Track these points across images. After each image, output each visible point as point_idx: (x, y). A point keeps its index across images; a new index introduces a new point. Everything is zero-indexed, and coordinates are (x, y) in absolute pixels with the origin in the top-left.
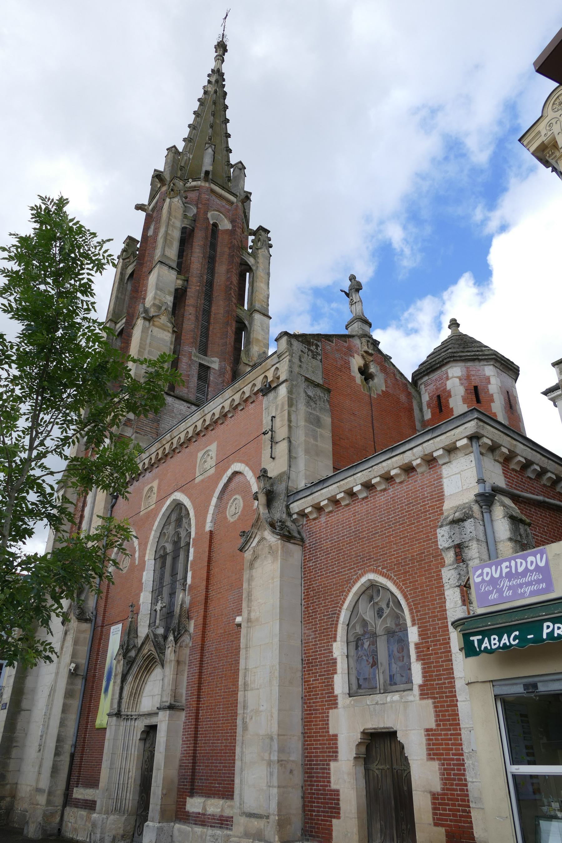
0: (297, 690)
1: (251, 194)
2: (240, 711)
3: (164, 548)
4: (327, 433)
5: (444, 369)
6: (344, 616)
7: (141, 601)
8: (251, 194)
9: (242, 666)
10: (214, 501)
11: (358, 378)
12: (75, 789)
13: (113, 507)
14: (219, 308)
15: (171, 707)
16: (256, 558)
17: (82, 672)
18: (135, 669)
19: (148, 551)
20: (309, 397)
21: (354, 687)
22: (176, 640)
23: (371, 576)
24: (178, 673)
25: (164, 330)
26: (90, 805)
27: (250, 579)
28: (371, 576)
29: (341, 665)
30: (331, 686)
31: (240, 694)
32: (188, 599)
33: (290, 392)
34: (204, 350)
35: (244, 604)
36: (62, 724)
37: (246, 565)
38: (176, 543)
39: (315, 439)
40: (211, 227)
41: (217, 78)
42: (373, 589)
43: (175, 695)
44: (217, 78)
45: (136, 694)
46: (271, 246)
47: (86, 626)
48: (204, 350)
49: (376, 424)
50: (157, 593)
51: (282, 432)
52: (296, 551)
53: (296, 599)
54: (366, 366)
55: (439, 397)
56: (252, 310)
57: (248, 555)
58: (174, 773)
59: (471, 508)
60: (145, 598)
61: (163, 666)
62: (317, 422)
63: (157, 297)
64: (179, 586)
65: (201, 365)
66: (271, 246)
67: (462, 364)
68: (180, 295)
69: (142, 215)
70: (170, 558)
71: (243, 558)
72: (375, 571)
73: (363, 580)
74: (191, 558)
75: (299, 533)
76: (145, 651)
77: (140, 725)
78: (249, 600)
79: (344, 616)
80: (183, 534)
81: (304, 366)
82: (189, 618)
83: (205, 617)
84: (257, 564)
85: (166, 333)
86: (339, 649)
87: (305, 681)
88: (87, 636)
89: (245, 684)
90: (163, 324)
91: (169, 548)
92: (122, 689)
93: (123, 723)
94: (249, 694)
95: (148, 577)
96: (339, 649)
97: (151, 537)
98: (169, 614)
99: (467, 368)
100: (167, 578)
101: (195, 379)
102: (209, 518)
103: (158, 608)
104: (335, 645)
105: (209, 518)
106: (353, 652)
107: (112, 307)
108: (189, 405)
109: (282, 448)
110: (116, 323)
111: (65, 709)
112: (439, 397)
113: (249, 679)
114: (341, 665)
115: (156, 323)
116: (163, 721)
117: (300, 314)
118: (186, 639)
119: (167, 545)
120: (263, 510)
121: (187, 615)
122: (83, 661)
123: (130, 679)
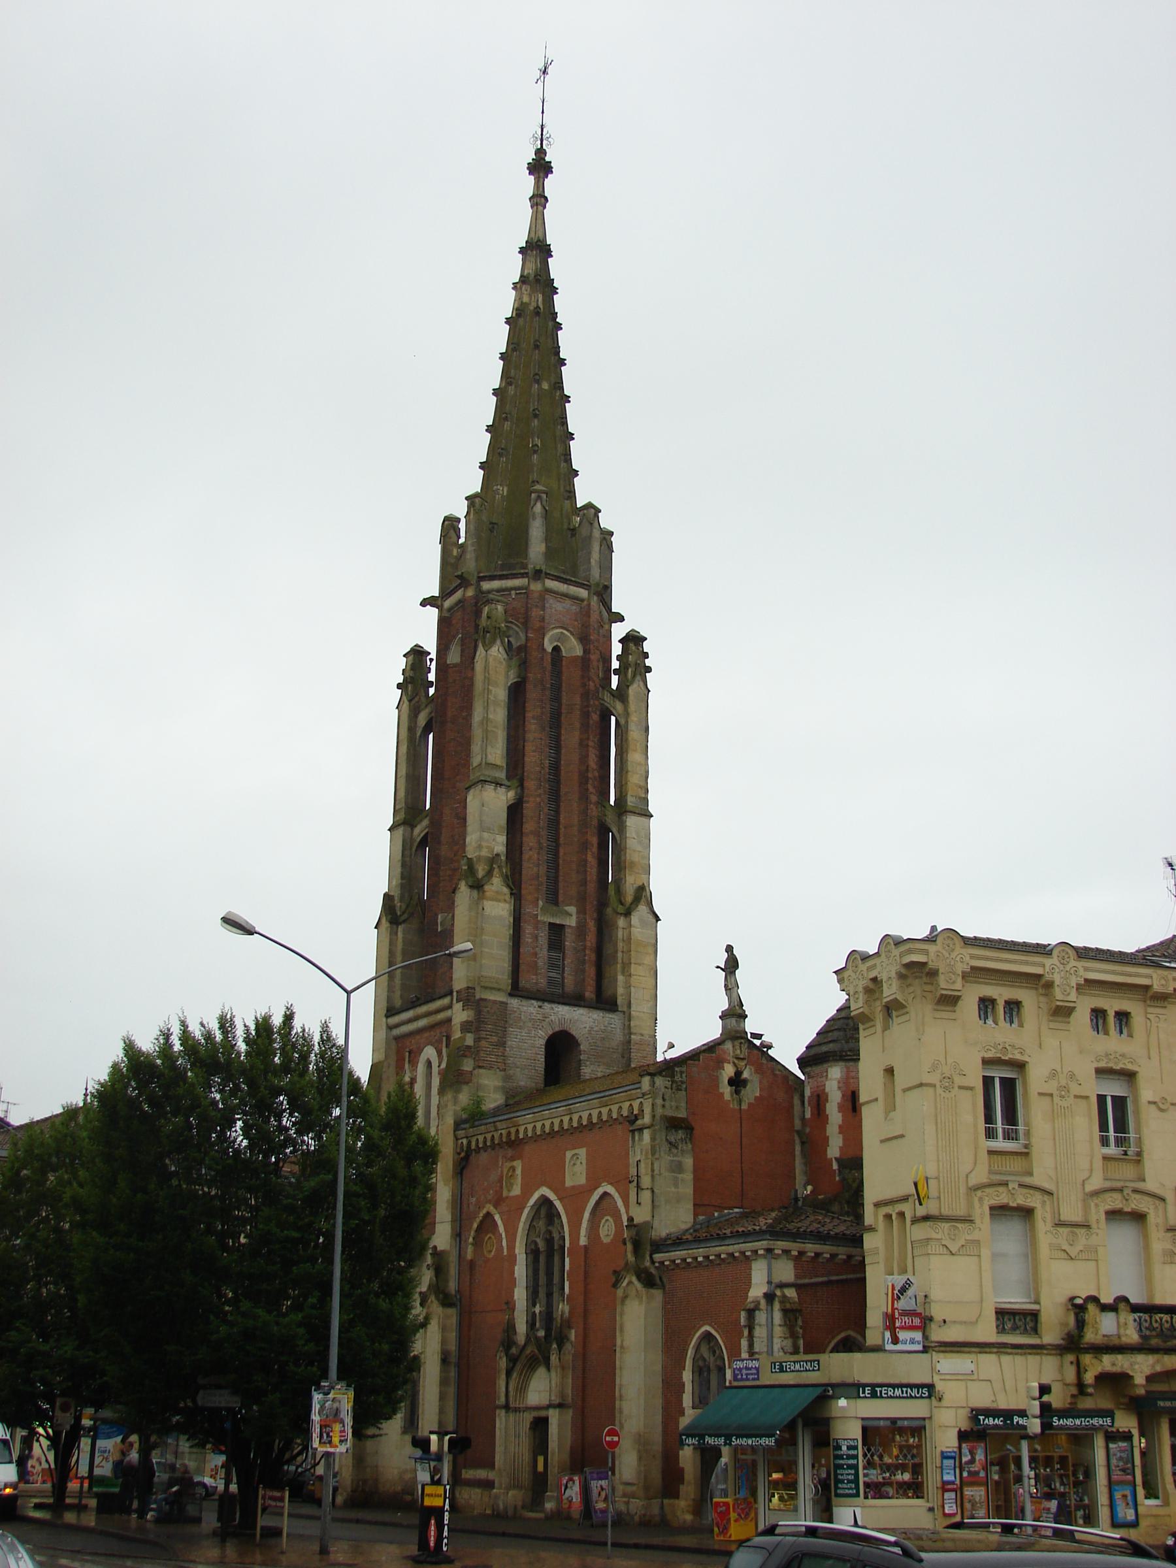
0: (658, 1402)
1: (612, 534)
2: (617, 1415)
3: (536, 1243)
4: (688, 1176)
5: (825, 1066)
6: (690, 1353)
7: (516, 1297)
8: (612, 534)
9: (618, 1381)
10: (587, 1215)
11: (726, 1091)
12: (463, 1471)
13: (463, 1169)
14: (570, 815)
15: (560, 1406)
16: (625, 1297)
17: (453, 1359)
18: (518, 1367)
19: (517, 1244)
20: (670, 1143)
21: (697, 1400)
22: (560, 1347)
23: (707, 1328)
24: (563, 1377)
25: (499, 901)
26: (488, 1485)
27: (622, 1314)
28: (707, 1328)
29: (688, 1388)
30: (680, 1401)
31: (617, 1402)
32: (567, 1309)
33: (653, 1139)
34: (553, 899)
35: (618, 1334)
36: (442, 1411)
37: (618, 1302)
38: (549, 1241)
39: (676, 1186)
40: (548, 659)
41: (537, 249)
42: (708, 1336)
43: (562, 1395)
44: (537, 249)
45: (523, 1389)
46: (649, 670)
47: (452, 1311)
48: (553, 899)
49: (744, 1140)
50: (533, 1298)
51: (646, 1181)
52: (658, 1294)
53: (658, 1337)
54: (738, 1073)
55: (818, 1096)
56: (622, 808)
57: (620, 1292)
58: (566, 1456)
59: (759, 1303)
60: (520, 1295)
61: (549, 1370)
62: (678, 1168)
63: (484, 844)
64: (556, 1296)
65: (552, 926)
66: (649, 670)
67: (842, 1064)
68: (515, 812)
69: (433, 613)
70: (546, 1255)
71: (615, 1293)
72: (710, 1325)
73: (703, 1329)
74: (567, 1267)
75: (661, 1278)
76: (528, 1351)
77: (528, 1417)
78: (622, 1331)
79: (690, 1353)
80: (556, 1236)
81: (667, 1104)
82: (570, 1327)
83: (585, 1329)
84: (627, 1302)
85: (501, 905)
86: (687, 1376)
87: (664, 1395)
88: (454, 1321)
89: (621, 1396)
90: (497, 892)
91: (541, 1245)
92: (507, 1384)
93: (512, 1416)
94: (624, 1403)
95: (520, 1271)
96: (687, 1376)
97: (520, 1229)
98: (548, 1316)
99: (848, 1068)
100: (542, 1279)
101: (545, 951)
102: (583, 1232)
103: (537, 1309)
104: (684, 1373)
105: (583, 1232)
106: (697, 1378)
107: (402, 794)
108: (540, 1003)
109: (646, 1196)
110: (413, 826)
111: (442, 1397)
112: (818, 1096)
113: (623, 1392)
114: (688, 1388)
115: (488, 894)
116: (554, 1416)
117: (654, 1083)
118: (568, 1347)
119: (538, 1240)
120: (631, 1258)
121: (567, 1324)
122: (453, 1347)
123: (515, 1375)
